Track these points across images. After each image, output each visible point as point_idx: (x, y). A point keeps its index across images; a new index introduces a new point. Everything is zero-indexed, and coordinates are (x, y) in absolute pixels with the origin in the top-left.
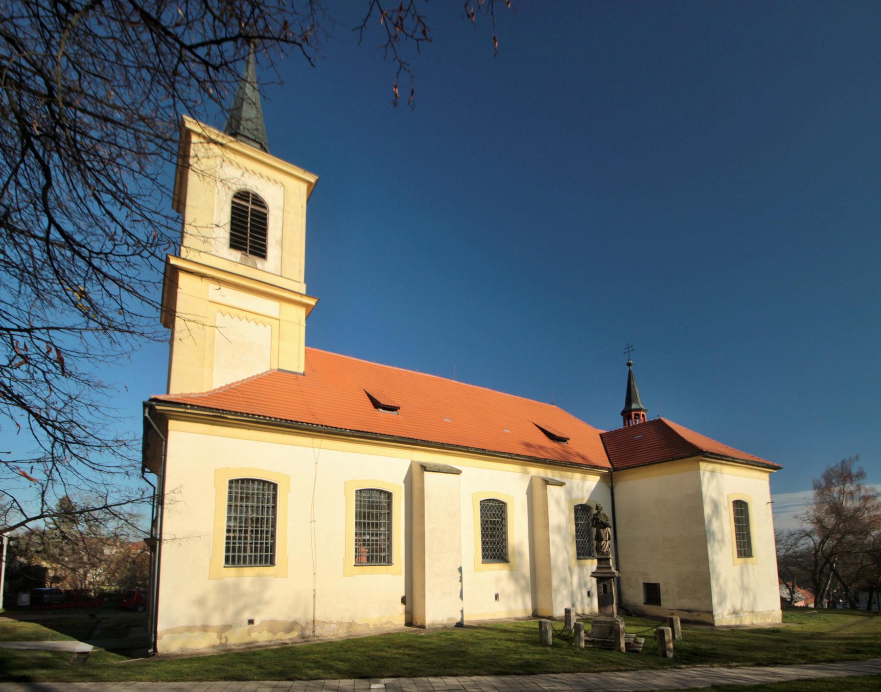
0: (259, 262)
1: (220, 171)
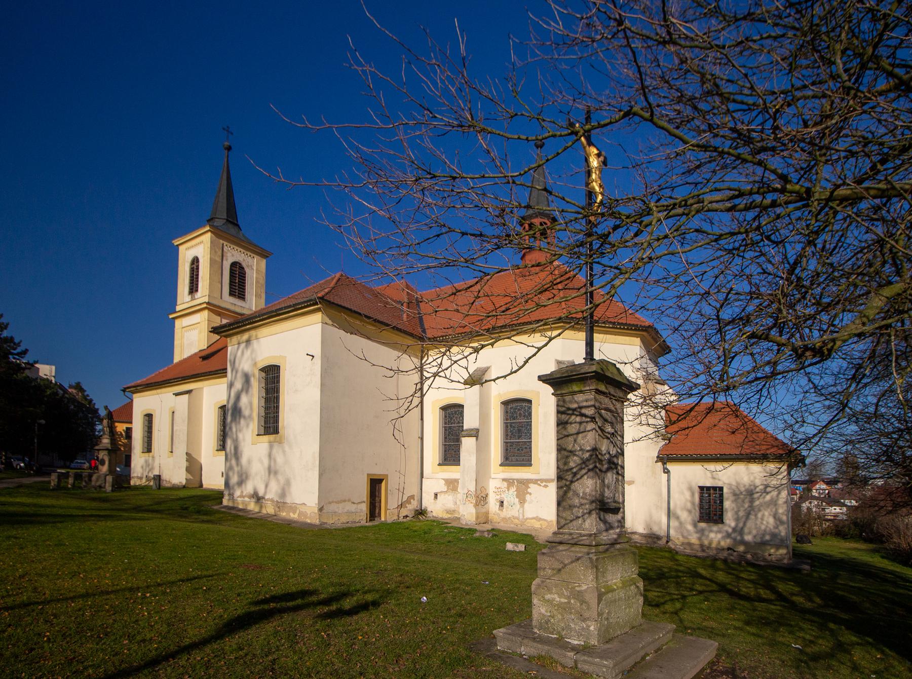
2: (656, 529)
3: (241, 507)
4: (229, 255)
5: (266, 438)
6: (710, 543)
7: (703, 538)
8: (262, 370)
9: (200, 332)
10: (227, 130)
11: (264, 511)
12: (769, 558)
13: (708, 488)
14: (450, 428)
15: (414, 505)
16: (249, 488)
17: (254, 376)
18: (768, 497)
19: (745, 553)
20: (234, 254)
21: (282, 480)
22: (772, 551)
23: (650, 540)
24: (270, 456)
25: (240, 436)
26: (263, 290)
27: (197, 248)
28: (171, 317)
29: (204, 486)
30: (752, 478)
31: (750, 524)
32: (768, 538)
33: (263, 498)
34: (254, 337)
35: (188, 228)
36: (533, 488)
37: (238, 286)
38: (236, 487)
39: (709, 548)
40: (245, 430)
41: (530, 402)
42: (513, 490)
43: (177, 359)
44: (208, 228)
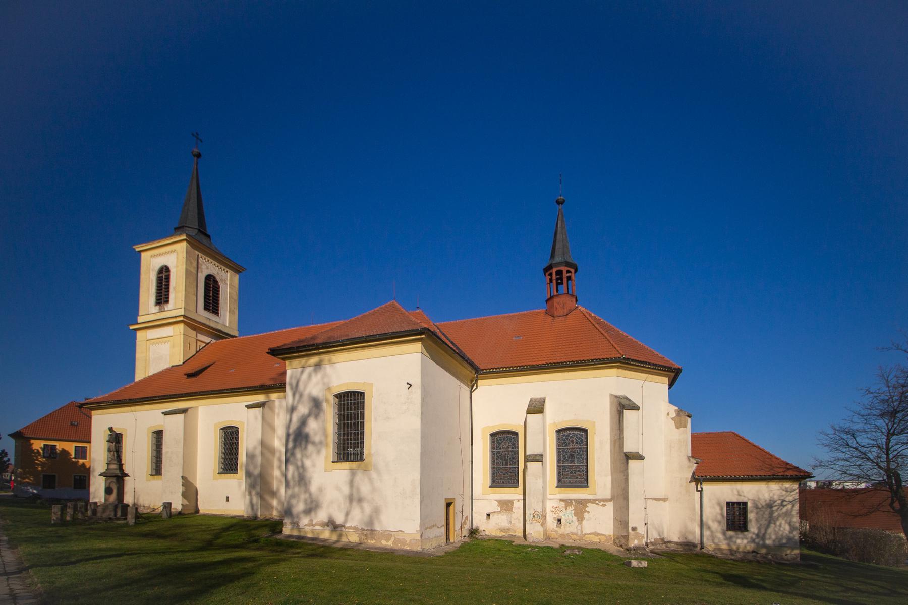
2: (690, 538)
3: (310, 535)
4: (204, 267)
5: (346, 465)
6: (738, 548)
7: (732, 544)
8: (336, 396)
9: (173, 346)
10: (196, 135)
11: (344, 540)
12: (786, 557)
13: (733, 503)
14: (498, 452)
15: (467, 527)
16: (322, 516)
17: (327, 401)
18: (784, 510)
19: (767, 554)
20: (209, 267)
21: (368, 508)
22: (789, 552)
23: (686, 547)
24: (351, 483)
25: (308, 463)
26: (236, 306)
27: (170, 255)
28: (131, 327)
29: (201, 512)
30: (771, 494)
31: (770, 530)
32: (784, 541)
33: (342, 526)
34: (326, 362)
35: (157, 233)
36: (590, 507)
37: (212, 302)
38: (302, 516)
39: (737, 551)
40: (314, 456)
41: (585, 431)
42: (571, 509)
43: (139, 376)
44: (184, 237)
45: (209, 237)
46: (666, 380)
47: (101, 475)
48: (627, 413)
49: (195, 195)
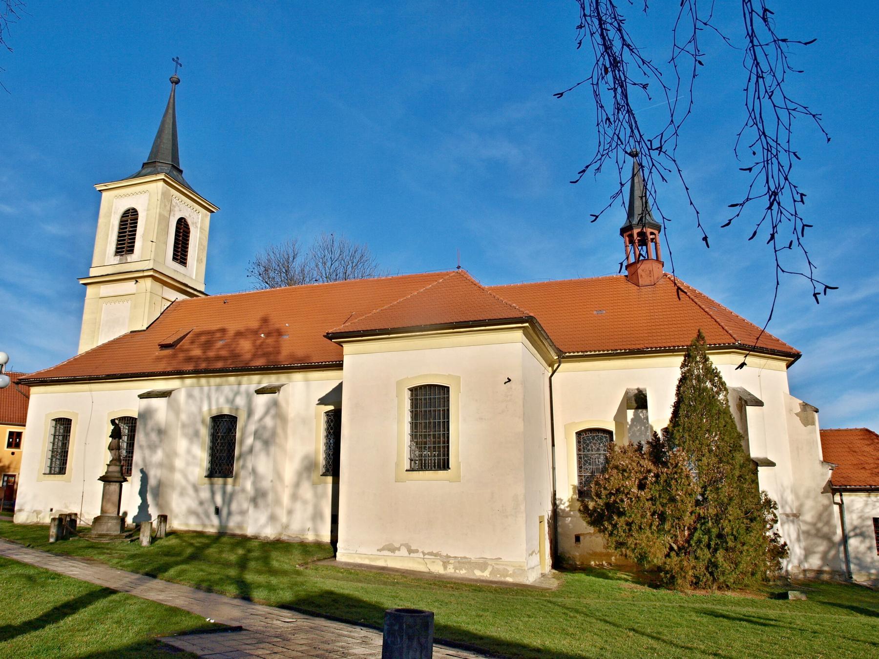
0: (130, 258)
1: (114, 203)
10: (176, 60)
45: (181, 172)
46: (783, 364)
47: (101, 479)
48: (750, 410)
49: (171, 126)
